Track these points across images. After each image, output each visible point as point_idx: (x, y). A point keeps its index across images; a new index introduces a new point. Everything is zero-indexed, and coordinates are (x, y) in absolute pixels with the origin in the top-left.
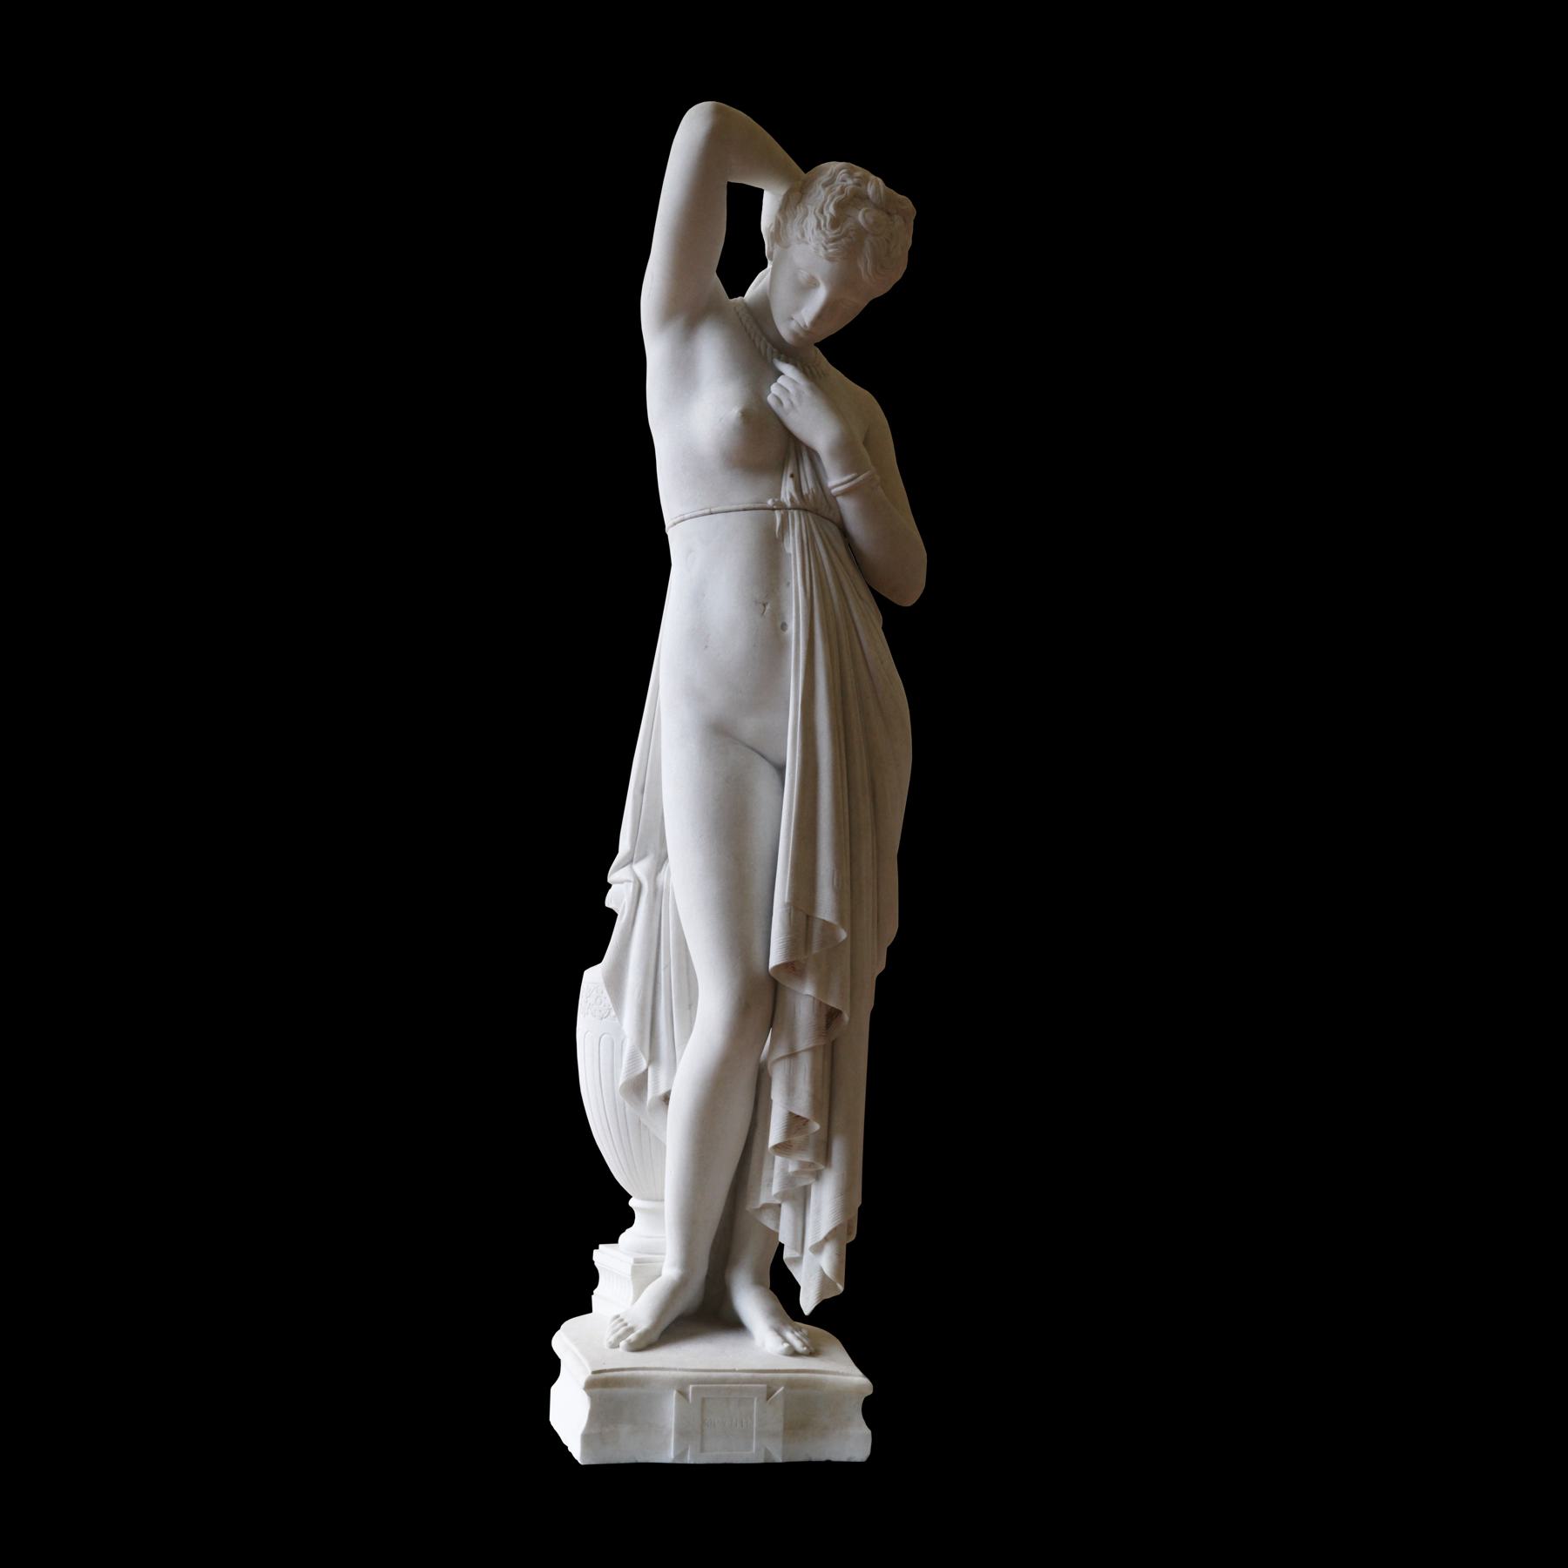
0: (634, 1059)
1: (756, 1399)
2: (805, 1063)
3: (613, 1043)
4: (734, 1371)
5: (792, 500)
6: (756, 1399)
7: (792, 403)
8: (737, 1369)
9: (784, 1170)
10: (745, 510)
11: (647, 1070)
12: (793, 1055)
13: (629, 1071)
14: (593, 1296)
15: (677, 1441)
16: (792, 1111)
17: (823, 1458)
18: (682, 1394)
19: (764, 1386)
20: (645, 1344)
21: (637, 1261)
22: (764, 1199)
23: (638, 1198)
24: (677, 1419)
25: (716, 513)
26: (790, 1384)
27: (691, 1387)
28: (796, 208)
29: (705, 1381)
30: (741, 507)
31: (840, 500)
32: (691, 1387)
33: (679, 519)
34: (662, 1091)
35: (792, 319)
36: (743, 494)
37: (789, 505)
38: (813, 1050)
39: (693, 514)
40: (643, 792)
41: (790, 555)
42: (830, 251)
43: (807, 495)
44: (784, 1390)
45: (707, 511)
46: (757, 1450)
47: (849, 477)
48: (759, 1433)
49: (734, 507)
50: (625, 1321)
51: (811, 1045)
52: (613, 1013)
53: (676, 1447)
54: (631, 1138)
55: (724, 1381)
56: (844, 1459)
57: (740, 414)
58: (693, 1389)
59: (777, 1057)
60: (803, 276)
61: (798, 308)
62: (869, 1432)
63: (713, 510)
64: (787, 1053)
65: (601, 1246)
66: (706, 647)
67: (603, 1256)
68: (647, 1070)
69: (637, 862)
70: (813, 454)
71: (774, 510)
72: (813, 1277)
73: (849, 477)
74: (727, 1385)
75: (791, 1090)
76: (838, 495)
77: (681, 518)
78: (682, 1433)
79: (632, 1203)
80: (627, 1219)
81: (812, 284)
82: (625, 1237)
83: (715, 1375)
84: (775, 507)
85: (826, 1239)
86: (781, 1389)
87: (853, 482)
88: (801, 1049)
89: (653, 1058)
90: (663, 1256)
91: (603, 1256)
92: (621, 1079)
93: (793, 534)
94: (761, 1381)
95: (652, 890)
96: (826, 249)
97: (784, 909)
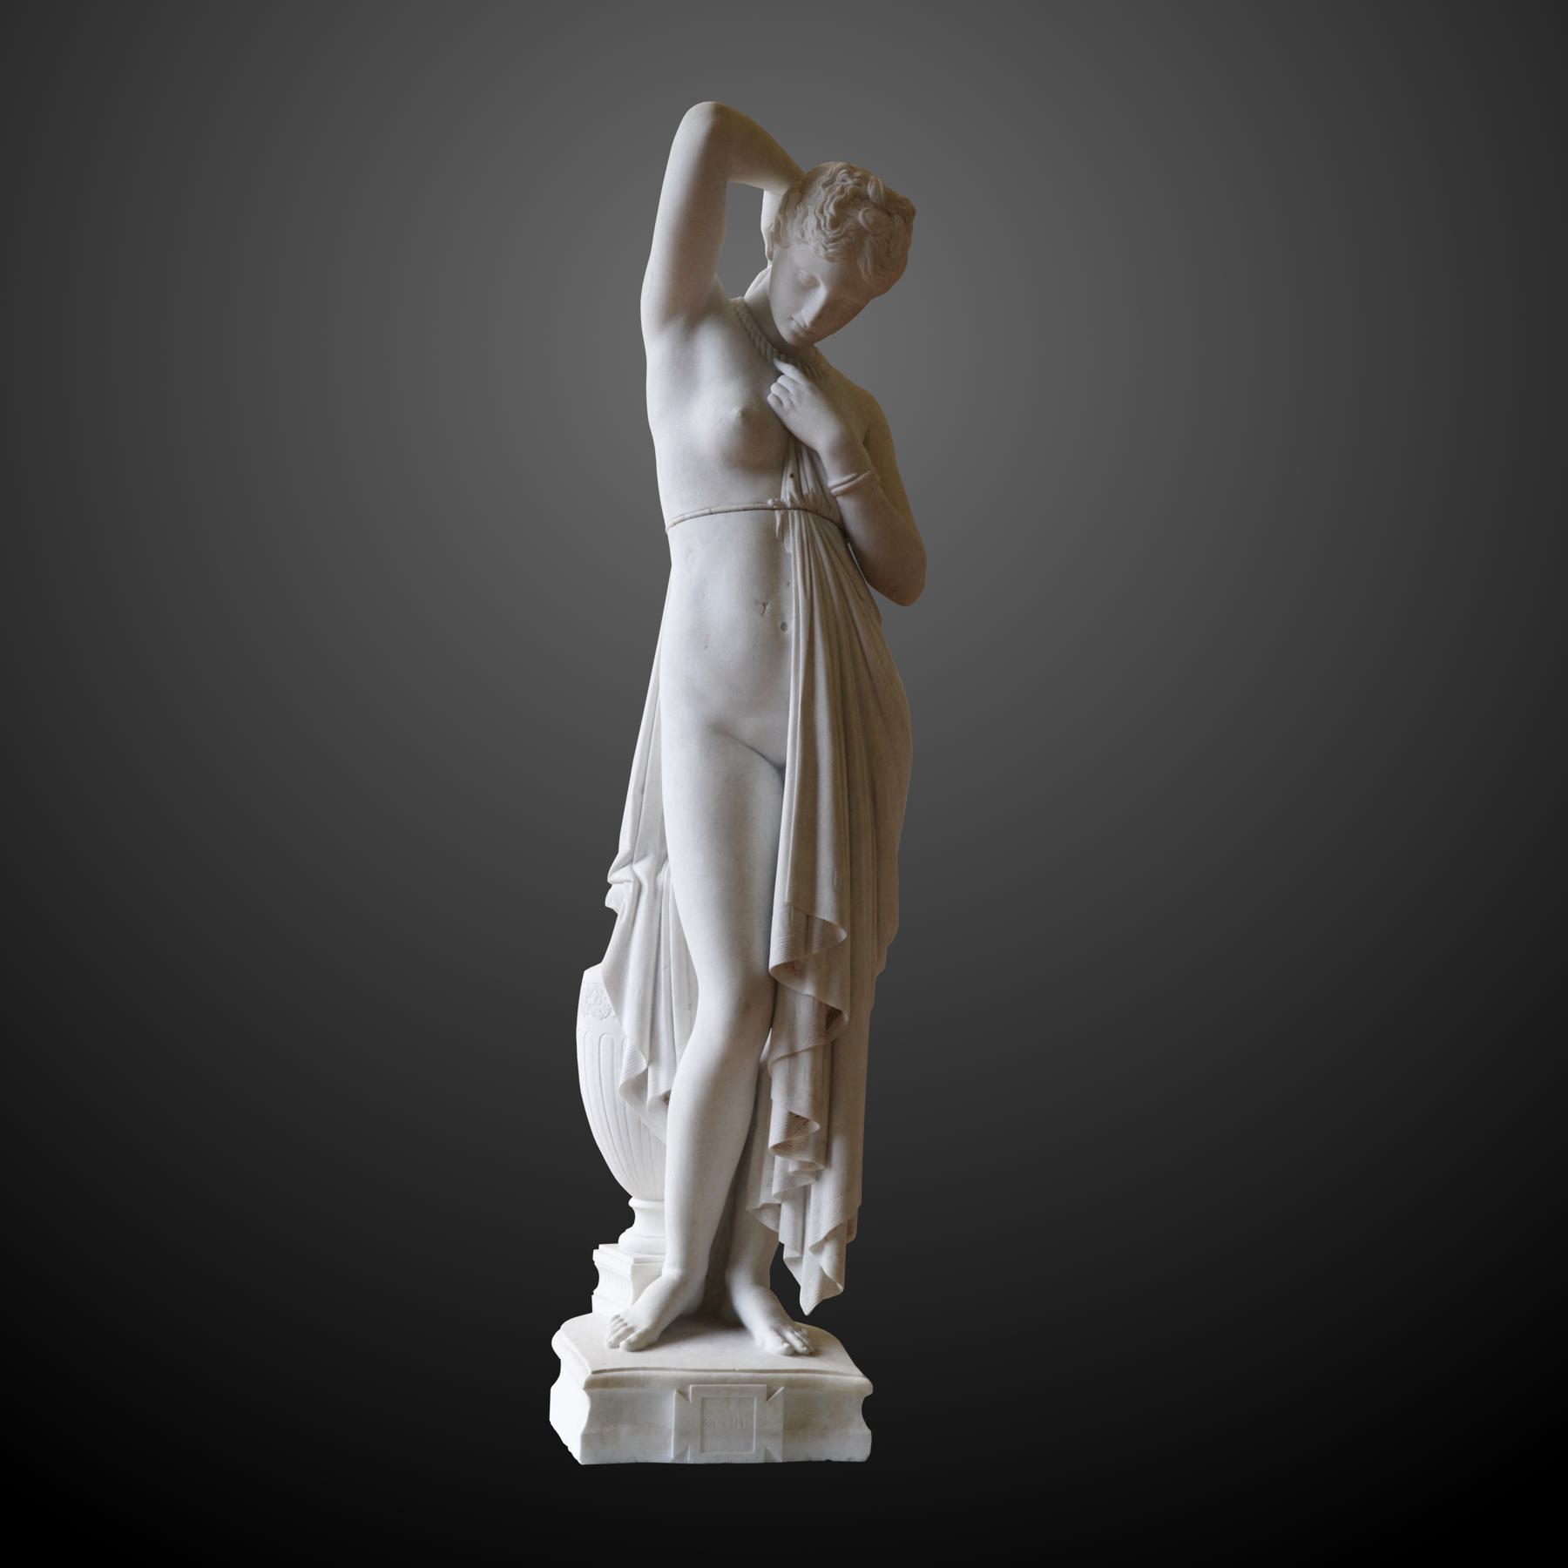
0: (634, 1059)
1: (756, 1399)
2: (805, 1063)
3: (613, 1043)
4: (734, 1371)
5: (792, 500)
6: (756, 1399)
7: (792, 403)
8: (737, 1369)
9: (784, 1170)
10: (745, 510)
11: (647, 1070)
12: (793, 1055)
13: (629, 1071)
14: (593, 1296)
15: (677, 1441)
16: (792, 1111)
17: (824, 1458)
18: (682, 1394)
19: (764, 1386)
20: (645, 1344)
21: (637, 1261)
22: (764, 1199)
23: (638, 1198)
24: (677, 1419)
25: (716, 513)
26: (790, 1384)
27: (691, 1387)
28: (796, 208)
29: (705, 1381)
30: (741, 507)
31: (840, 500)
32: (691, 1387)
33: (679, 519)
34: (662, 1091)
35: (792, 319)
36: (743, 494)
37: (789, 505)
38: (813, 1050)
39: (693, 514)
40: (643, 792)
41: (790, 555)
42: (830, 251)
43: (807, 495)
44: (784, 1390)
45: (707, 511)
46: (757, 1450)
47: (849, 477)
48: (759, 1433)
49: (734, 507)
50: (625, 1321)
51: (811, 1045)
52: (613, 1013)
53: (676, 1447)
54: (631, 1138)
55: (724, 1381)
56: (844, 1459)
57: (740, 414)
58: (693, 1389)
59: (777, 1057)
60: (803, 276)
61: (798, 308)
62: (868, 1432)
63: (713, 510)
64: (787, 1053)
65: (601, 1246)
66: (706, 647)
67: (603, 1256)
68: (647, 1070)
69: (637, 862)
70: (813, 454)
71: (774, 510)
72: (813, 1277)
73: (849, 477)
74: (727, 1385)
75: (791, 1090)
76: (838, 495)
77: (681, 518)
78: (682, 1433)
79: (632, 1203)
80: (627, 1219)
81: (812, 284)
82: (625, 1237)
83: (715, 1375)
84: (775, 507)
85: (826, 1239)
86: (781, 1389)
87: (853, 482)
88: (801, 1049)
89: (653, 1058)
90: (663, 1256)
91: (603, 1256)
92: (621, 1079)
93: (793, 534)
94: (761, 1381)
95: (652, 890)
96: (826, 249)
97: (784, 909)
